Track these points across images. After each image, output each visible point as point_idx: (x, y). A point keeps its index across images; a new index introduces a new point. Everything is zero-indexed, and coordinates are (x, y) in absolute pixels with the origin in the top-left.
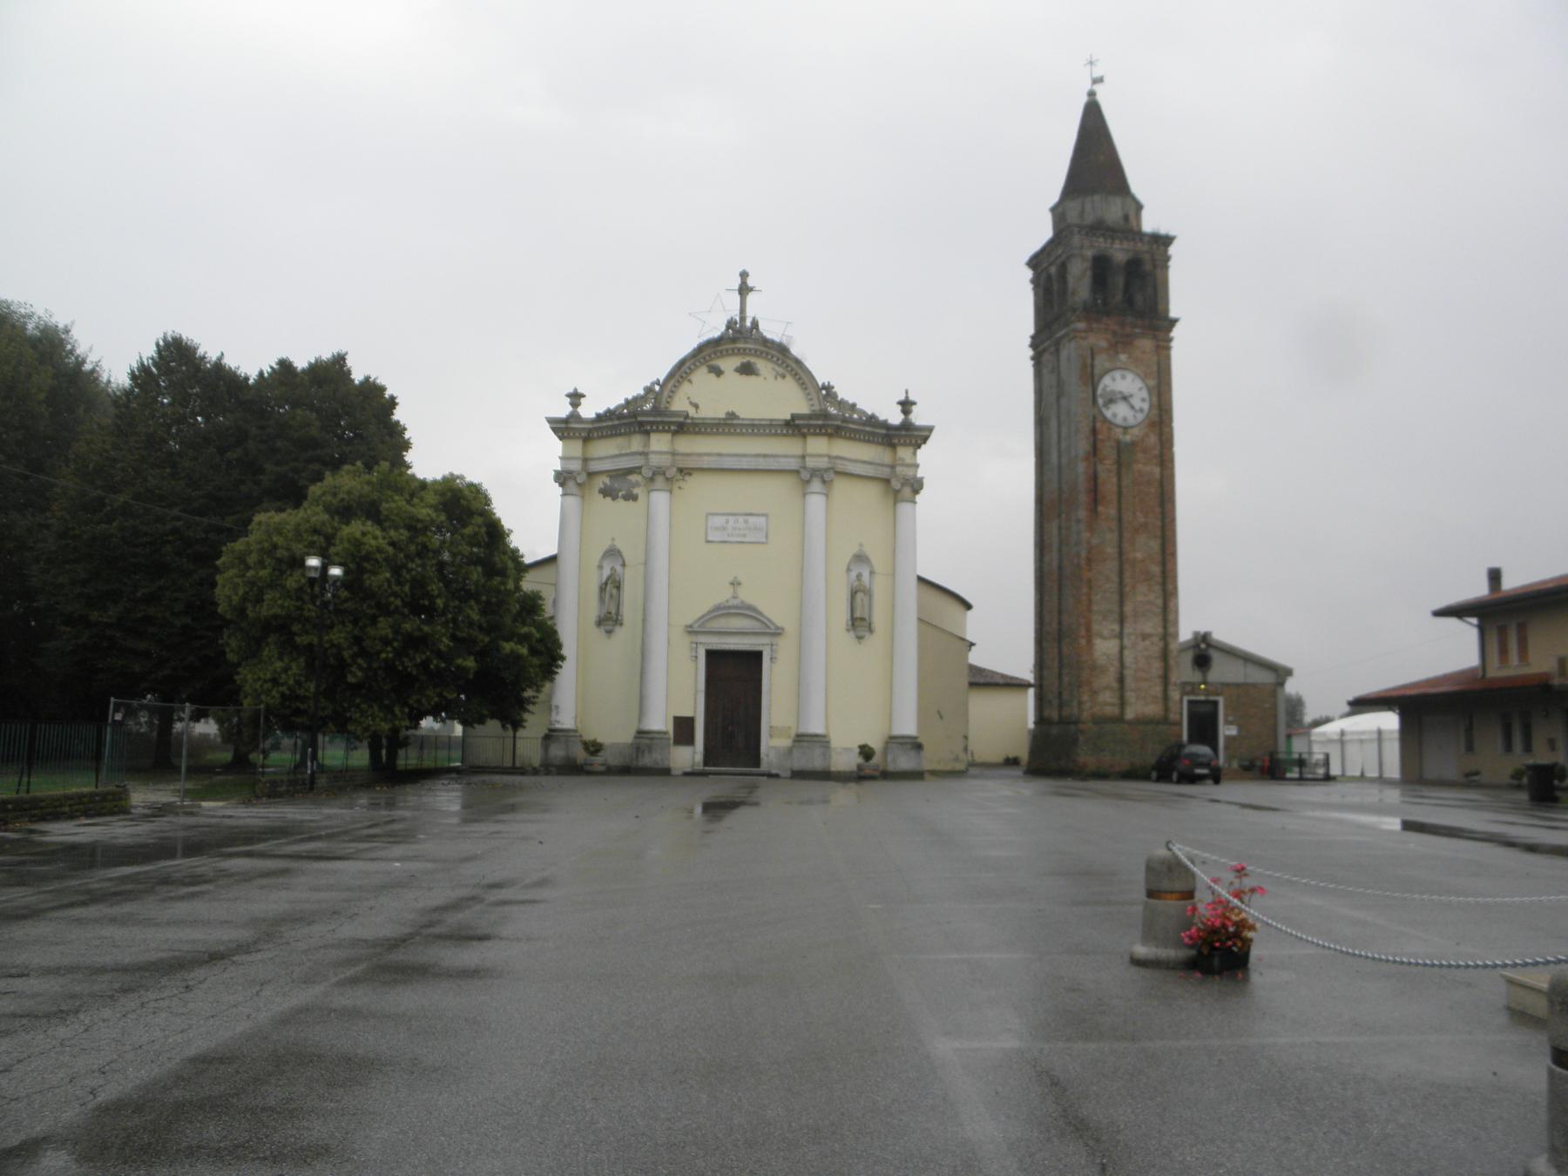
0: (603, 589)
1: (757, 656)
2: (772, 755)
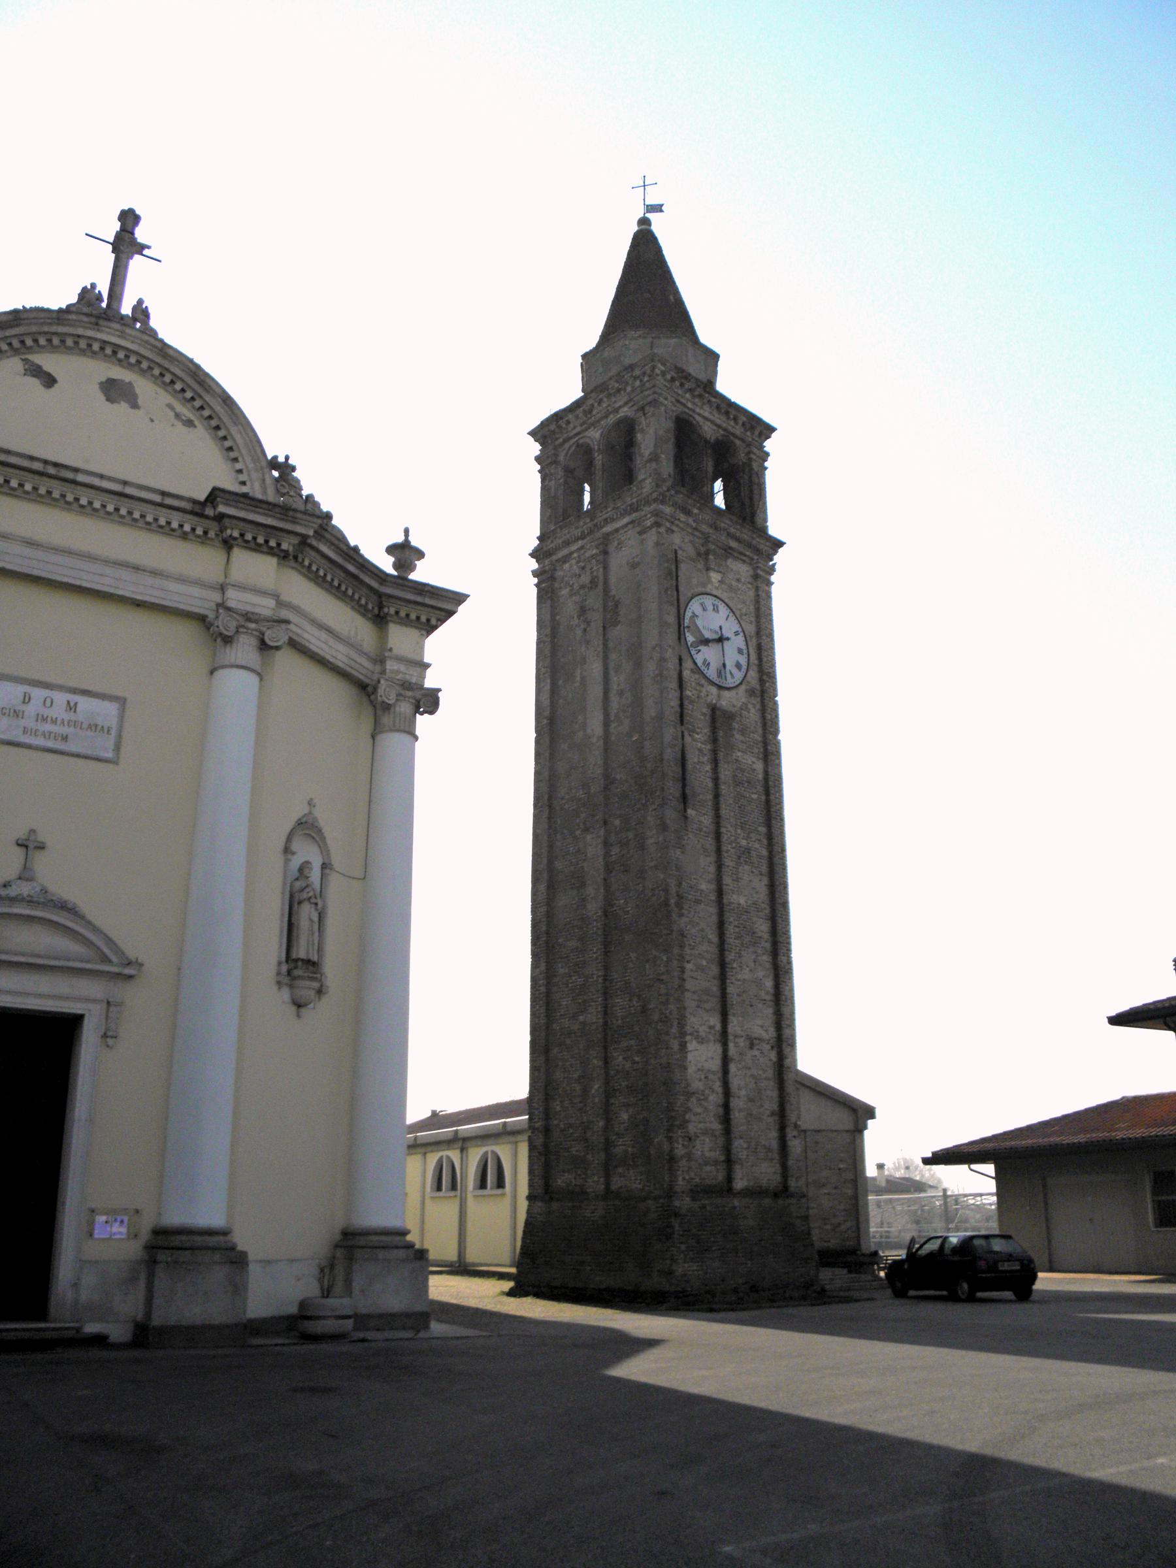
1: (69, 1026)
2: (89, 1279)
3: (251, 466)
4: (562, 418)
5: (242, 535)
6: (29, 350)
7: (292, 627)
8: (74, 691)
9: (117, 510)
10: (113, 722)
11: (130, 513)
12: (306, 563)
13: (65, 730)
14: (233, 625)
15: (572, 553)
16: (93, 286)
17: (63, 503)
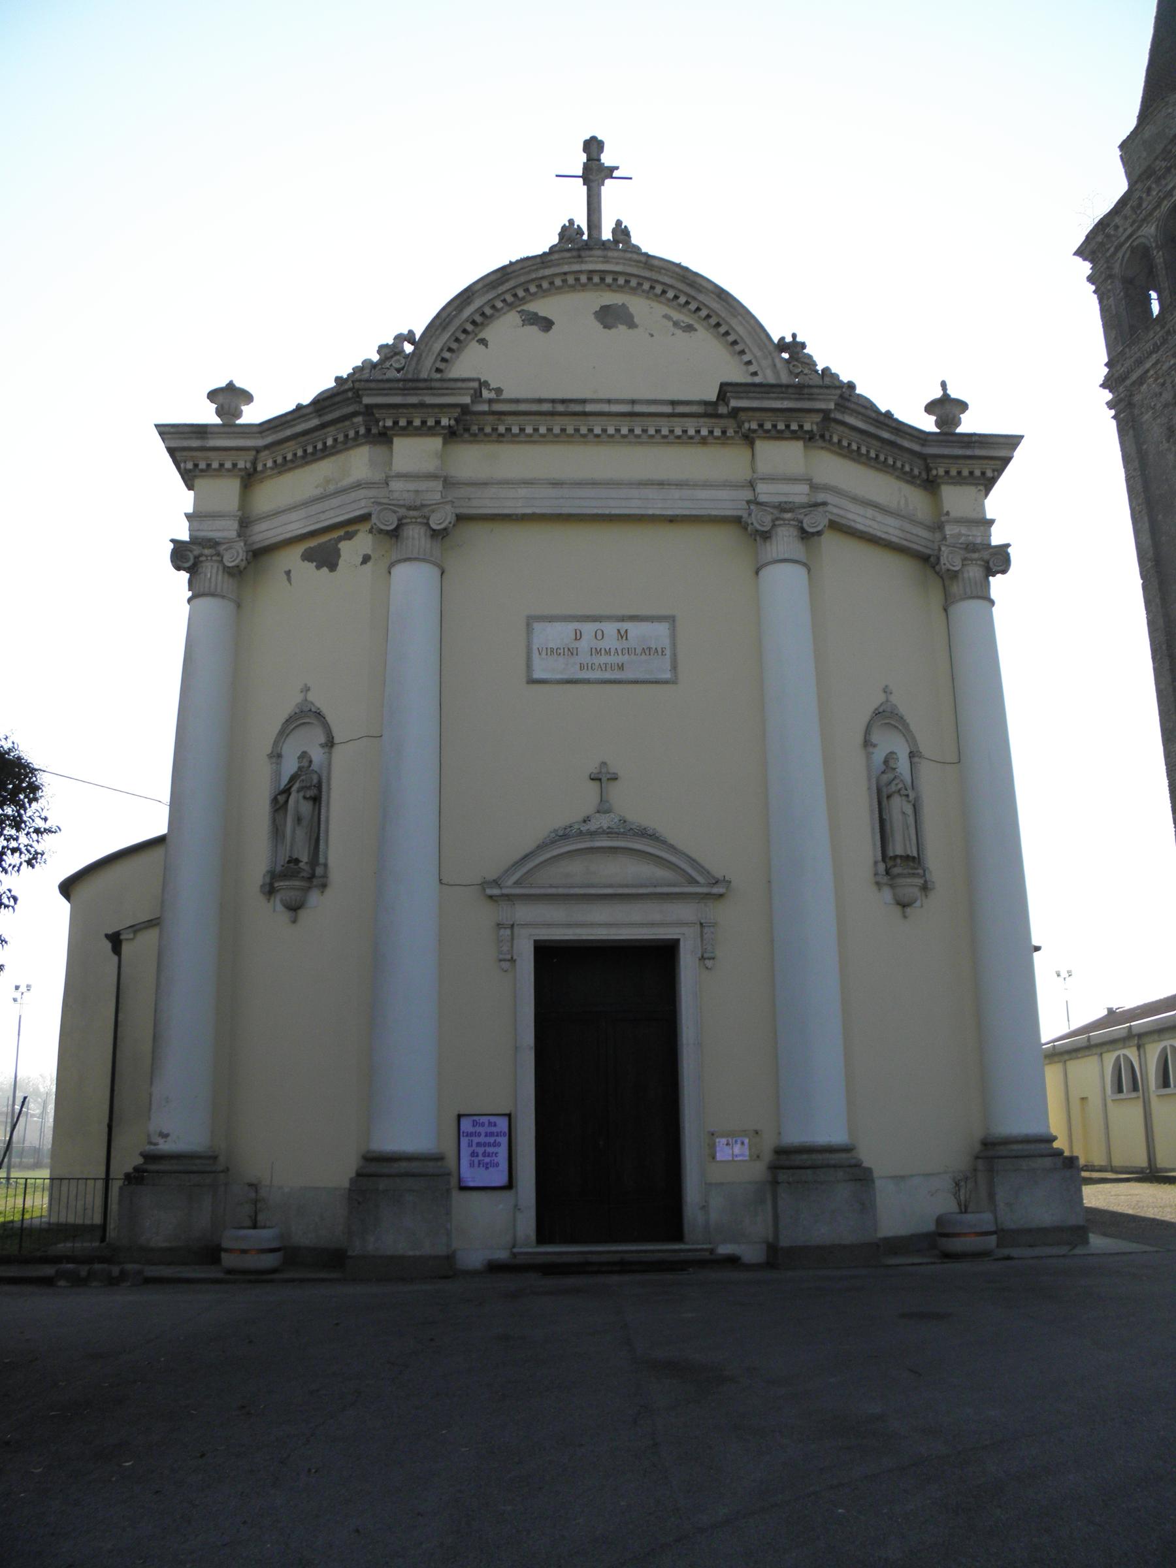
0: (279, 803)
1: (663, 954)
3: (759, 354)
4: (1108, 225)
5: (761, 426)
6: (523, 300)
7: (829, 508)
8: (623, 619)
9: (631, 431)
10: (666, 642)
11: (645, 431)
12: (835, 439)
13: (620, 659)
14: (768, 519)
15: (1148, 371)
16: (571, 222)
17: (578, 438)
